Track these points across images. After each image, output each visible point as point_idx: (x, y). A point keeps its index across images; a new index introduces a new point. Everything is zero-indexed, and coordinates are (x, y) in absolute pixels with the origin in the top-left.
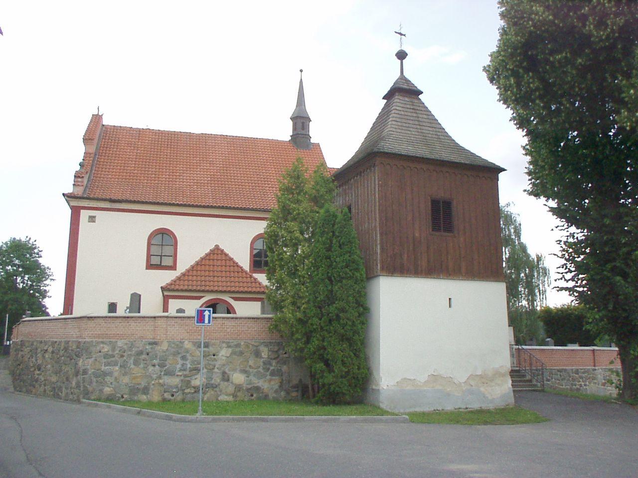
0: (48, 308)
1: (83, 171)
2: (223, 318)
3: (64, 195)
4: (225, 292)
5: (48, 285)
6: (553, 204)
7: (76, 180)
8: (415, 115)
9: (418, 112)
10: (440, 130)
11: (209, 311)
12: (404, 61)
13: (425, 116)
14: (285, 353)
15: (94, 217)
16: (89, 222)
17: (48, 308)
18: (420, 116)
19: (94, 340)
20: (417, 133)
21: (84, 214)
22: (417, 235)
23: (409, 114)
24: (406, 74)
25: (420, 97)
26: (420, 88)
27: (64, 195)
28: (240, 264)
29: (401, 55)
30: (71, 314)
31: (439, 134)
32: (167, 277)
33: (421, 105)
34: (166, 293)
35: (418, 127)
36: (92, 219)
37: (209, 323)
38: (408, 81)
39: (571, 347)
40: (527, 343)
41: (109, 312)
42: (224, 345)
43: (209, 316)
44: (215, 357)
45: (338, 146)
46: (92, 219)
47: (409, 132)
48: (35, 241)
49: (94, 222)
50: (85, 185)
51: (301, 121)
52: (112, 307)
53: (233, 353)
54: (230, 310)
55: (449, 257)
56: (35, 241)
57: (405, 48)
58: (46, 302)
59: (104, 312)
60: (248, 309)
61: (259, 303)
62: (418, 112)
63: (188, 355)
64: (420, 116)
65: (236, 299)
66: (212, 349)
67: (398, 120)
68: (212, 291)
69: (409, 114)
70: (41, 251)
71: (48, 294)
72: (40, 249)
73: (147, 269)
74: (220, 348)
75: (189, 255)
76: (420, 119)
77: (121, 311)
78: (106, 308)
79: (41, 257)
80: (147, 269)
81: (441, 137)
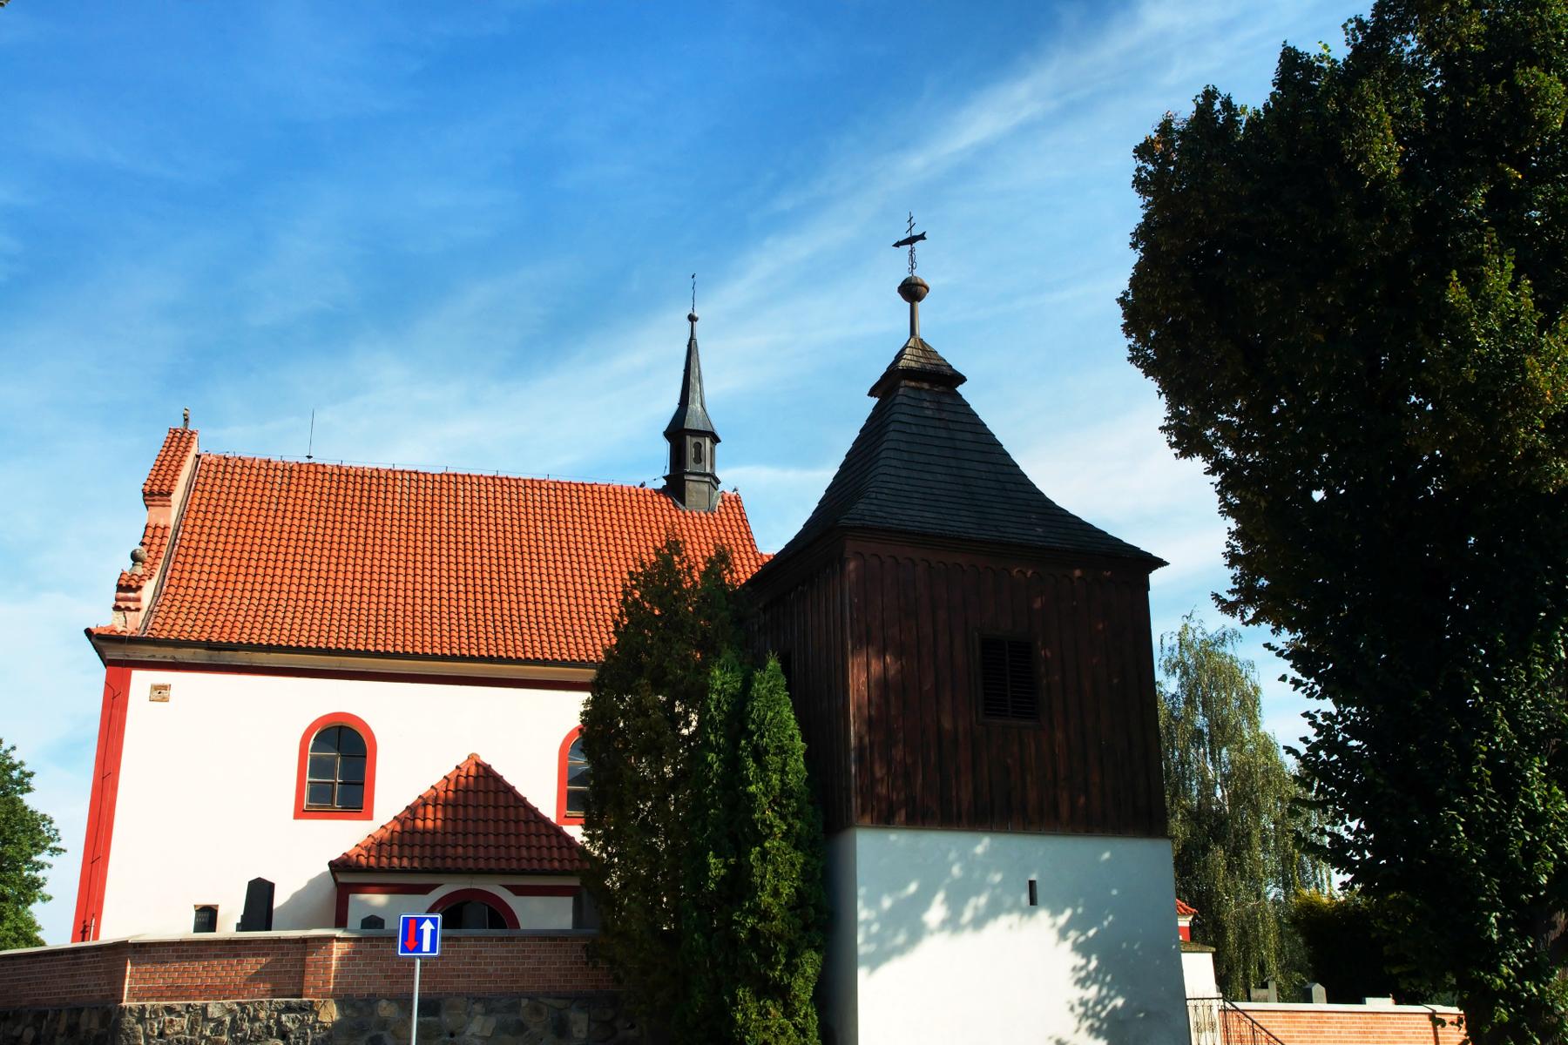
0: (39, 929)
1: (140, 570)
2: (478, 939)
3: (88, 632)
4: (490, 872)
5: (42, 867)
6: (1284, 638)
7: (122, 595)
8: (944, 434)
9: (951, 425)
10: (1006, 469)
11: (434, 921)
12: (920, 305)
13: (969, 436)
14: (632, 1027)
15: (166, 687)
16: (1210, 95)
17: (39, 929)
18: (959, 436)
19: (148, 1004)
20: (948, 479)
21: (141, 681)
22: (947, 724)
23: (931, 432)
24: (922, 332)
25: (960, 389)
26: (959, 366)
27: (88, 632)
28: (533, 800)
29: (912, 291)
30: (96, 937)
31: (1001, 478)
32: (344, 836)
33: (961, 409)
34: (342, 879)
35: (953, 463)
36: (160, 691)
37: (433, 949)
38: (924, 347)
39: (1373, 1004)
40: (1253, 994)
41: (196, 930)
42: (478, 1007)
43: (433, 933)
44: (455, 1039)
45: (775, 497)
46: (160, 691)
47: (927, 476)
48: (13, 748)
49: (165, 700)
50: (145, 609)
51: (686, 439)
52: (207, 917)
53: (502, 1028)
54: (500, 917)
55: (1029, 778)
56: (13, 748)
57: (921, 274)
58: (37, 910)
59: (182, 927)
60: (546, 914)
61: (568, 902)
62: (951, 425)
63: (385, 1034)
64: (959, 436)
65: (519, 891)
66: (447, 1019)
67: (903, 446)
68: (457, 872)
69: (931, 432)
70: (30, 775)
71: (45, 890)
72: (27, 769)
73: (301, 813)
74: (469, 1014)
75: (400, 783)
76: (958, 444)
77: (228, 927)
78: (190, 919)
79: (29, 790)
80: (301, 813)
81: (1009, 486)
